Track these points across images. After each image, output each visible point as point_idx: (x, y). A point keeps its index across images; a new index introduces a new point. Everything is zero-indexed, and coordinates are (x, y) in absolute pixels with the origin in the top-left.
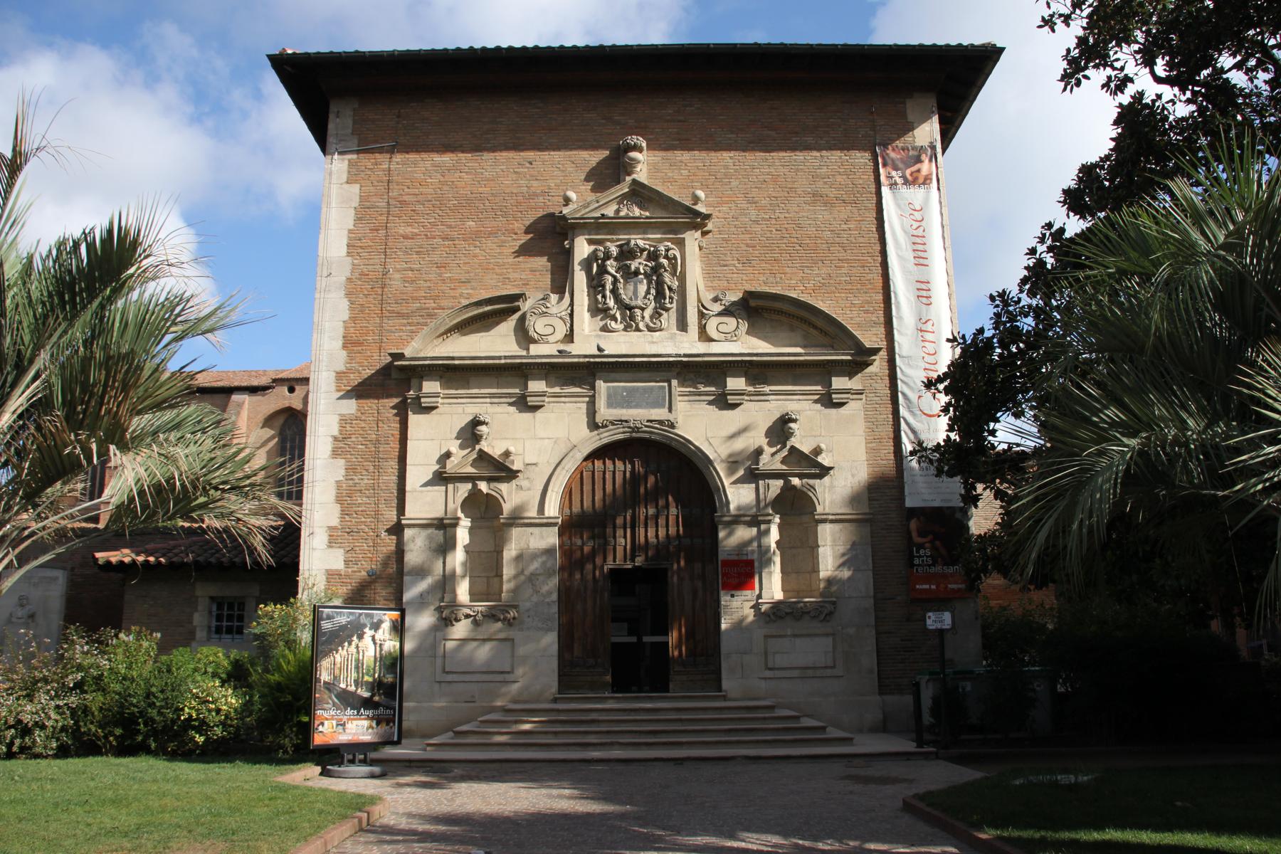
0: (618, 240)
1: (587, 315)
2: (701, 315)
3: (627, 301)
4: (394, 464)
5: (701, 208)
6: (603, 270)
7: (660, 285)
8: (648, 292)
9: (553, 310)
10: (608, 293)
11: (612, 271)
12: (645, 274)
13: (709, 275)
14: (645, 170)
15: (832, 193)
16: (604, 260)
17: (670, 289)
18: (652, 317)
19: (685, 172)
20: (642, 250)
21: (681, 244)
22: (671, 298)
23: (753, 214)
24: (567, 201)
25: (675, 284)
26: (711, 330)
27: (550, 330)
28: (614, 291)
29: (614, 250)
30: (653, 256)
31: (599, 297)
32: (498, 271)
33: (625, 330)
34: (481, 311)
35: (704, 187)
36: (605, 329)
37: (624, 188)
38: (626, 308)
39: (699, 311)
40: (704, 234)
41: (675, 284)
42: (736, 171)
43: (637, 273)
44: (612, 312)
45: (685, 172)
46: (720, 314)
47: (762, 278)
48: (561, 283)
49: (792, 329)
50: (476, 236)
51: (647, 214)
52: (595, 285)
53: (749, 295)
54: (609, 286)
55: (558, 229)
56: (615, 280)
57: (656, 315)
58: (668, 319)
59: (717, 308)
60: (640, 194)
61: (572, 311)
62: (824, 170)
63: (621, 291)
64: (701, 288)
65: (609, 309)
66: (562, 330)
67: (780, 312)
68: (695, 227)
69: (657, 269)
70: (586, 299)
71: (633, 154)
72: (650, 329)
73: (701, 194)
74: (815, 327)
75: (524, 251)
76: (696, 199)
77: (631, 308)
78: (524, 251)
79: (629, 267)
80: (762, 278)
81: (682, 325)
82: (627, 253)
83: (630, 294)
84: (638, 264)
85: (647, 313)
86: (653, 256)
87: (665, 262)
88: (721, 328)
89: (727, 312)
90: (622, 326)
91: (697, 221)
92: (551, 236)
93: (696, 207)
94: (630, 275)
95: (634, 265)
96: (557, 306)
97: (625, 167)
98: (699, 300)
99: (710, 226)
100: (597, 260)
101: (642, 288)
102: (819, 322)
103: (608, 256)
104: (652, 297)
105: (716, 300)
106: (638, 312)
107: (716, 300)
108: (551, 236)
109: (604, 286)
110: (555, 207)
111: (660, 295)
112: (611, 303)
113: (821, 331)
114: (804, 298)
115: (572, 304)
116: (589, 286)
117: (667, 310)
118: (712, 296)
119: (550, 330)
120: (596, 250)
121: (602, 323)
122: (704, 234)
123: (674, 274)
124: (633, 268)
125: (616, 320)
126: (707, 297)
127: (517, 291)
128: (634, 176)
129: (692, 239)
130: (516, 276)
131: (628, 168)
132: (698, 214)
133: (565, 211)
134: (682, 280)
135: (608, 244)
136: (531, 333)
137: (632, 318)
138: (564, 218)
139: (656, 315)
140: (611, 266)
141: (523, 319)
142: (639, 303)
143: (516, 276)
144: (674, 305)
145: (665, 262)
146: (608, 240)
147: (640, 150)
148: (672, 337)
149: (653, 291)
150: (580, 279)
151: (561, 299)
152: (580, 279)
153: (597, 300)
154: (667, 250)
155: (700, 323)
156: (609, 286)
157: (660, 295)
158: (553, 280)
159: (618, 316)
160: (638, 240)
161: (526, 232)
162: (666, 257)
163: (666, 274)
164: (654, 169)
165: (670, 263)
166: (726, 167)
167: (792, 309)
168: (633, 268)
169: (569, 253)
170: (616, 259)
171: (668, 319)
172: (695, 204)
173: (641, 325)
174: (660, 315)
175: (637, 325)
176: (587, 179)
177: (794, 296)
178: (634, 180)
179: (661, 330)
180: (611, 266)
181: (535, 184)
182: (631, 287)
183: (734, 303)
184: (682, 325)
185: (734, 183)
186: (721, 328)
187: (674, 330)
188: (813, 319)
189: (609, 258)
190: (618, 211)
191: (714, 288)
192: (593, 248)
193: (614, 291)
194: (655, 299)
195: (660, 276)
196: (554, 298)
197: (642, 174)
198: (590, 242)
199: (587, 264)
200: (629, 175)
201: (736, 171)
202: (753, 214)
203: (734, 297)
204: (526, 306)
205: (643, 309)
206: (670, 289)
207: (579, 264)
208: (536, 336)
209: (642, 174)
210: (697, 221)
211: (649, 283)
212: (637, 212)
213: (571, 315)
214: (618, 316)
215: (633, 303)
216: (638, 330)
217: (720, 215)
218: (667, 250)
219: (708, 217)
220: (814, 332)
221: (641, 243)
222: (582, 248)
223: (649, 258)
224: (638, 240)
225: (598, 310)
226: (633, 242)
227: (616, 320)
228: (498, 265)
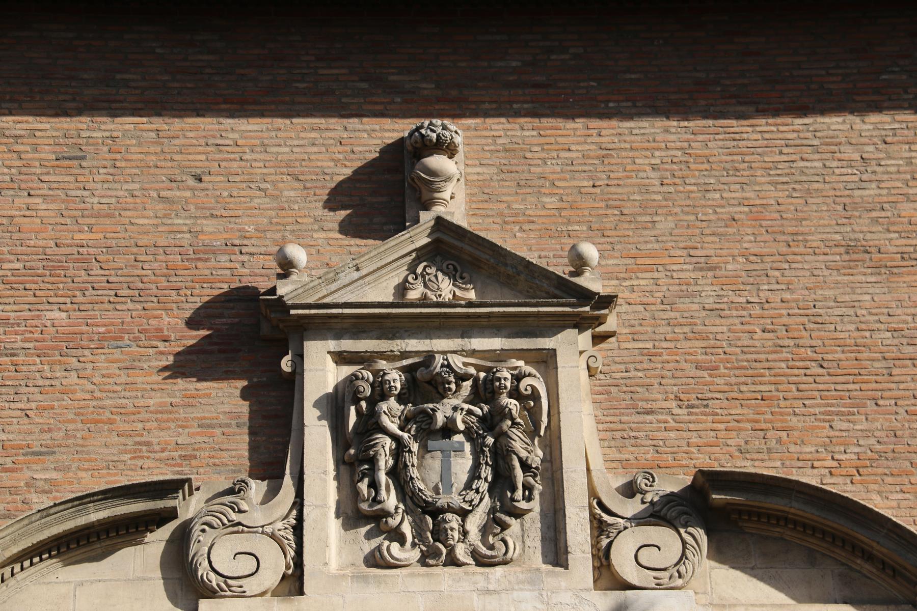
0: (404, 355)
1: (334, 526)
2: (599, 527)
3: (428, 495)
4: (451, 320)
5: (590, 281)
6: (371, 424)
7: (501, 457)
8: (474, 474)
9: (256, 516)
10: (383, 477)
11: (394, 427)
12: (468, 433)
13: (612, 432)
14: (461, 196)
15: (892, 243)
16: (373, 401)
17: (526, 466)
18: (485, 531)
19: (551, 202)
20: (461, 378)
21: (546, 361)
22: (527, 487)
23: (709, 293)
24: (286, 267)
25: (536, 457)
26: (623, 562)
27: (248, 565)
28: (398, 473)
29: (396, 378)
30: (485, 391)
31: (363, 486)
32: (125, 427)
33: (423, 561)
34: (81, 521)
35: (597, 234)
36: (376, 560)
37: (419, 236)
38: (427, 511)
39: (593, 515)
40: (598, 339)
41: (536, 457)
42: (667, 196)
43: (448, 430)
44: (393, 522)
45: (551, 202)
46: (640, 520)
47: (735, 441)
48: (273, 454)
49: (812, 559)
50: (70, 343)
51: (472, 295)
52: (354, 458)
53: (709, 480)
54: (385, 462)
55: (265, 329)
56: (400, 448)
57: (495, 524)
58: (525, 535)
59: (633, 507)
60: (452, 249)
61: (300, 519)
62: (872, 191)
63: (414, 473)
64: (597, 464)
65: (388, 514)
66: (275, 563)
67: (783, 519)
68: (581, 323)
69: (493, 421)
70: (332, 485)
71: (437, 161)
72: (482, 561)
73: (590, 251)
74: (868, 556)
75: (187, 365)
76: (579, 263)
77: (436, 512)
78: (187, 365)
79: (430, 417)
80: (735, 441)
81: (556, 552)
82: (424, 384)
83: (435, 478)
84: (452, 408)
85: (474, 524)
86: (485, 391)
87: (513, 405)
88: (646, 557)
89: (662, 513)
90: (416, 554)
91: (584, 309)
92: (248, 338)
93: (581, 281)
94: (430, 431)
95: (442, 413)
96: (264, 509)
97: (416, 190)
98: (593, 493)
99: (611, 323)
100: (356, 401)
101: (462, 465)
102: (881, 546)
103: (381, 391)
104: (484, 487)
105: (630, 490)
106: (454, 521)
107: (630, 490)
108: (248, 338)
109: (373, 461)
110: (258, 274)
111: (502, 482)
112: (391, 500)
113: (884, 566)
114: (838, 486)
115: (299, 503)
116: (341, 461)
117: (519, 514)
118: (620, 481)
119: (248, 565)
120: (354, 378)
121: (368, 546)
122: (598, 339)
123: (533, 432)
124: (440, 419)
125: (402, 542)
126: (609, 484)
127: (167, 475)
128: (439, 210)
129: (571, 347)
130: (164, 436)
131: (423, 193)
132: (585, 296)
133: (284, 289)
134: (553, 447)
135: (382, 364)
136: (203, 570)
137: (440, 534)
138: (280, 305)
139: (495, 524)
140: (391, 413)
141: (181, 541)
142: (456, 500)
143: (164, 436)
144: (535, 505)
145: (513, 405)
146: (382, 355)
147: (450, 150)
148: (534, 580)
149: (487, 472)
150: (318, 439)
151: (273, 492)
152: (318, 439)
153: (356, 493)
154: (518, 378)
155: (595, 545)
156: (385, 462)
157: (502, 482)
158: (253, 448)
159: (407, 529)
160: (451, 351)
161: (192, 323)
162: (515, 393)
163: (516, 433)
164: (481, 193)
165: (524, 408)
166: (645, 189)
167: (810, 514)
168: (440, 419)
169: (292, 384)
170: (401, 399)
171: (525, 535)
172: (578, 273)
173: (461, 552)
174: (504, 527)
175: (451, 550)
176: (334, 201)
177: (814, 482)
178: (439, 221)
179: (505, 563)
180: (391, 413)
181: (209, 225)
182: (434, 463)
183: (670, 498)
184: (556, 552)
185: (665, 224)
186: (646, 557)
187: (536, 557)
188: (862, 536)
189: (384, 397)
190: (402, 288)
191: (625, 465)
192: (347, 371)
193: (398, 473)
194: (490, 490)
195: (501, 436)
196: (257, 488)
197: (455, 204)
198: (341, 358)
199: (334, 406)
200: (427, 207)
201: (667, 196)
202: (709, 293)
203: (672, 483)
204: (190, 507)
205: (464, 514)
206: (526, 466)
207: (317, 404)
208: (214, 580)
209: (455, 204)
210: (584, 309)
211: (477, 453)
212: (446, 288)
213: (298, 529)
214: (407, 529)
215: (442, 501)
216: (453, 561)
217: (634, 297)
218: (518, 378)
219: (607, 301)
220: (867, 567)
221: (457, 362)
222: (322, 370)
223: (475, 398)
224: (451, 351)
225: (357, 514)
226: (439, 360)
227: (402, 542)
228: (121, 411)
